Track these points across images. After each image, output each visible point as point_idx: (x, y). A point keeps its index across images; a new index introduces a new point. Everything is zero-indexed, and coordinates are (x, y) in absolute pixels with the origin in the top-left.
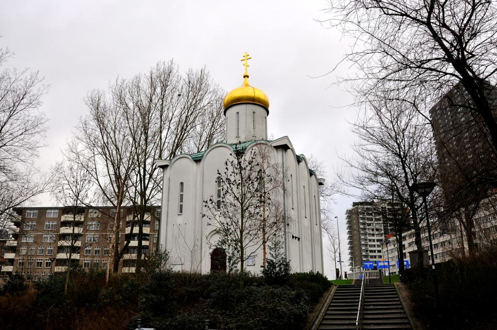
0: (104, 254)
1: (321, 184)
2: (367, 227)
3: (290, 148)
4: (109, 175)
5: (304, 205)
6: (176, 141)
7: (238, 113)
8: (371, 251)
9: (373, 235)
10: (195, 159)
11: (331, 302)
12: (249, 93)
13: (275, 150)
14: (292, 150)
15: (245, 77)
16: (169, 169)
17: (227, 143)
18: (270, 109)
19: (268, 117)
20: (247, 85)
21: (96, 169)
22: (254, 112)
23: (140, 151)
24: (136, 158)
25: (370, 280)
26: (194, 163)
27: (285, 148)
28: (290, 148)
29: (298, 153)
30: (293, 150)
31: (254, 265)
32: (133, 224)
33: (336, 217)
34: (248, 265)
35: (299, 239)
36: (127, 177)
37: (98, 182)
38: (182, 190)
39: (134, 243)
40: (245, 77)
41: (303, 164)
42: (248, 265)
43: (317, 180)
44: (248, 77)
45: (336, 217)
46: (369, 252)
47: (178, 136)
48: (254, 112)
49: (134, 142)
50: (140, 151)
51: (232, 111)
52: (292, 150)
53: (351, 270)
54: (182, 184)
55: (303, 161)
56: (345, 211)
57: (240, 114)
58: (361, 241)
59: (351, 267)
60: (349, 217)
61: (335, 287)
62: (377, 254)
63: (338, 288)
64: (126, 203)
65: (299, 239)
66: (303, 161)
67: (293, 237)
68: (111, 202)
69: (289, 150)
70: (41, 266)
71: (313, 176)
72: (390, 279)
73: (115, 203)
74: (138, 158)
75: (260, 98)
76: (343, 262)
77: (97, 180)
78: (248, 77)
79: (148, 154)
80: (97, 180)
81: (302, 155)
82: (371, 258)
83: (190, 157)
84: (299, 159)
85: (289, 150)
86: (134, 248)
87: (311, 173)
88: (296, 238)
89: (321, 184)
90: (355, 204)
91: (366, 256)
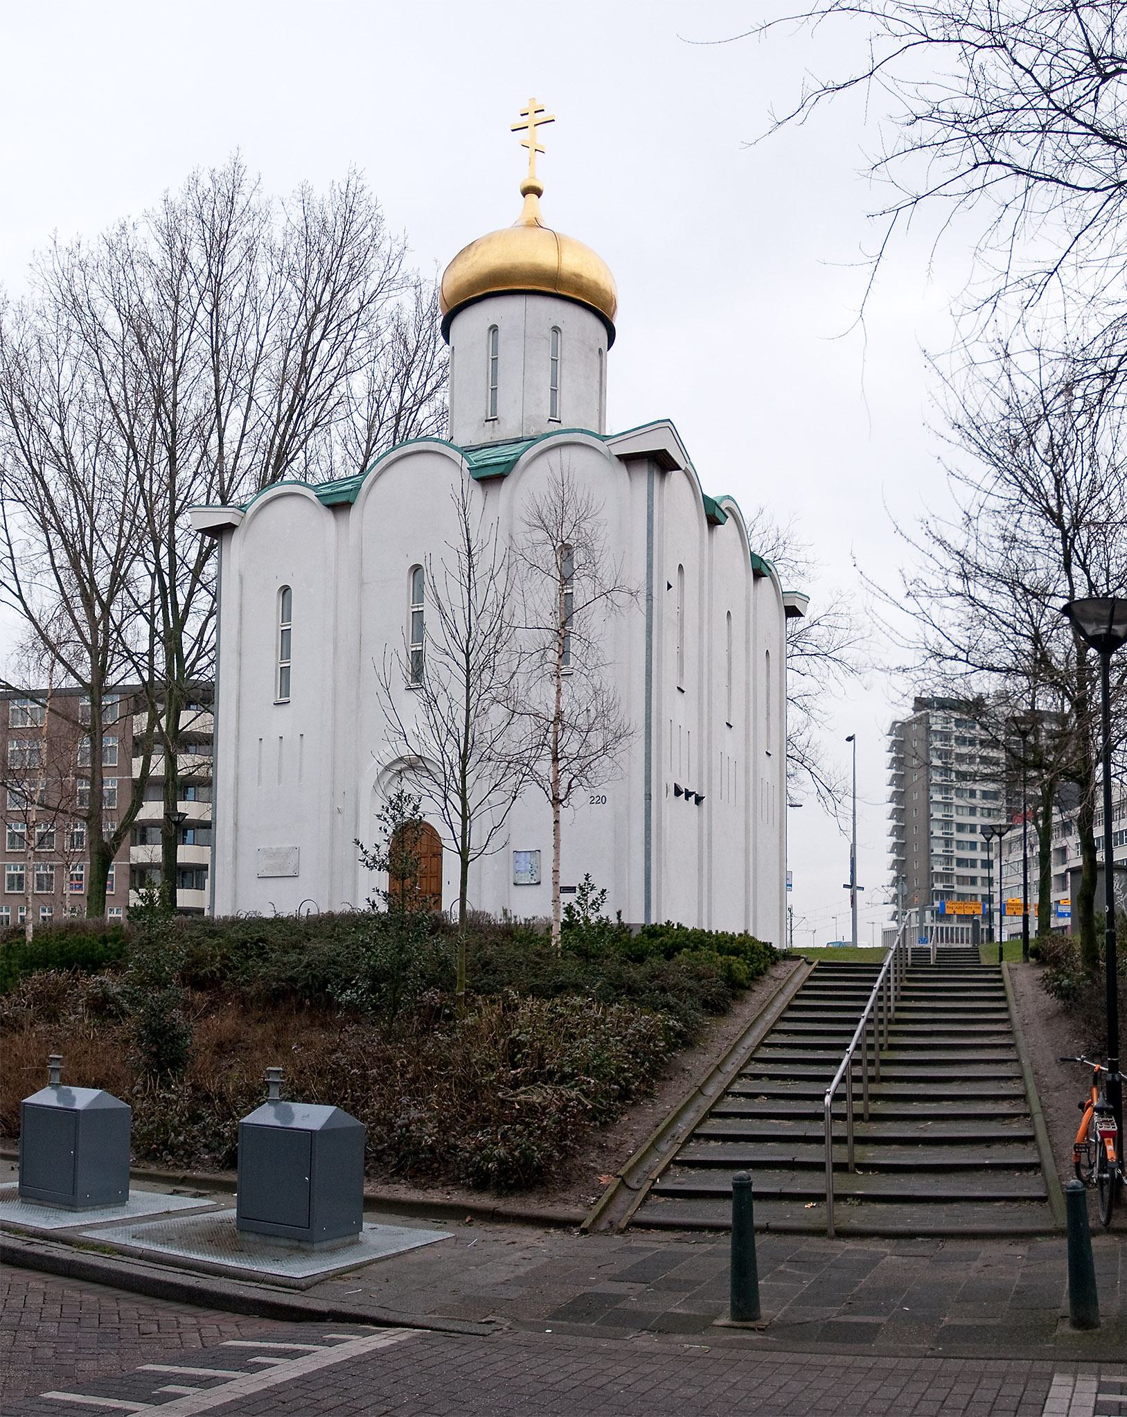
0: (72, 846)
1: (792, 612)
2: (956, 801)
3: (679, 469)
4: (55, 569)
5: (725, 682)
6: (277, 441)
7: (494, 329)
8: (961, 862)
9: (973, 811)
10: (328, 502)
11: (782, 1019)
12: (543, 256)
13: (622, 470)
14: (686, 472)
15: (526, 192)
16: (237, 537)
17: (454, 442)
18: (617, 323)
19: (612, 355)
20: (535, 224)
21: (12, 558)
22: (556, 329)
23: (155, 487)
24: (142, 512)
25: (939, 950)
26: (328, 516)
27: (661, 462)
28: (679, 469)
29: (712, 491)
30: (691, 478)
31: (539, 883)
32: (142, 746)
33: (849, 739)
34: (515, 884)
35: (699, 800)
36: (119, 581)
37: (24, 604)
38: (286, 615)
39: (152, 810)
40: (526, 192)
41: (727, 530)
42: (515, 884)
43: (780, 594)
44: (538, 192)
45: (849, 739)
46: (954, 866)
47: (281, 429)
48: (556, 329)
49: (131, 452)
50: (155, 487)
51: (472, 323)
52: (686, 472)
53: (893, 919)
54: (285, 590)
55: (730, 521)
56: (887, 727)
57: (501, 333)
58: (934, 842)
59: (893, 908)
60: (897, 746)
61: (806, 967)
62: (980, 872)
63: (816, 970)
64: (123, 675)
65: (699, 800)
66: (730, 521)
67: (678, 792)
68: (70, 670)
69: (675, 474)
70: (20, 887)
71: (765, 581)
72: (1001, 949)
73: (85, 670)
74: (150, 512)
75: (579, 276)
76: (845, 886)
77: (20, 597)
78: (538, 192)
79: (182, 497)
80: (20, 597)
81: (729, 497)
82: (958, 865)
83: (311, 494)
84: (714, 515)
85: (675, 473)
86: (153, 823)
87: (760, 570)
88: (688, 795)
89: (792, 612)
90: (920, 703)
91: (946, 877)
